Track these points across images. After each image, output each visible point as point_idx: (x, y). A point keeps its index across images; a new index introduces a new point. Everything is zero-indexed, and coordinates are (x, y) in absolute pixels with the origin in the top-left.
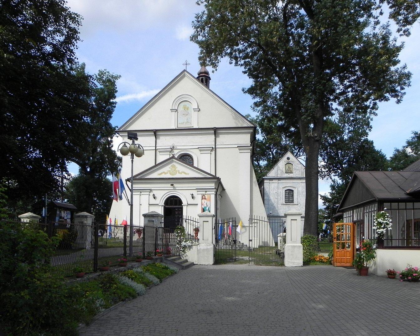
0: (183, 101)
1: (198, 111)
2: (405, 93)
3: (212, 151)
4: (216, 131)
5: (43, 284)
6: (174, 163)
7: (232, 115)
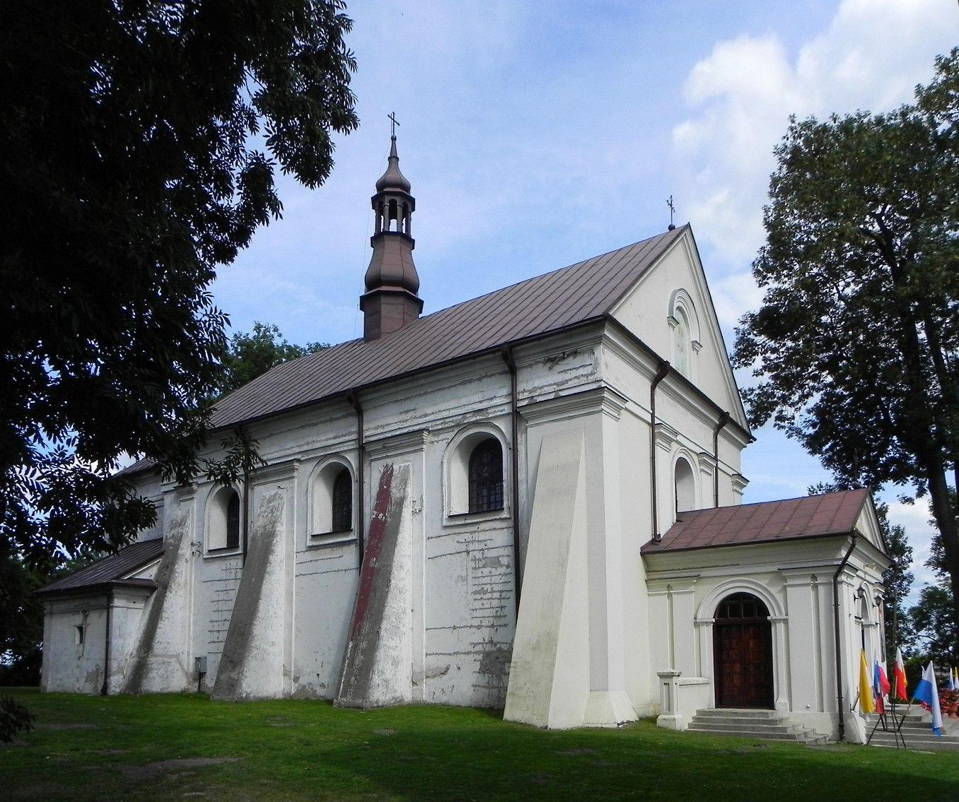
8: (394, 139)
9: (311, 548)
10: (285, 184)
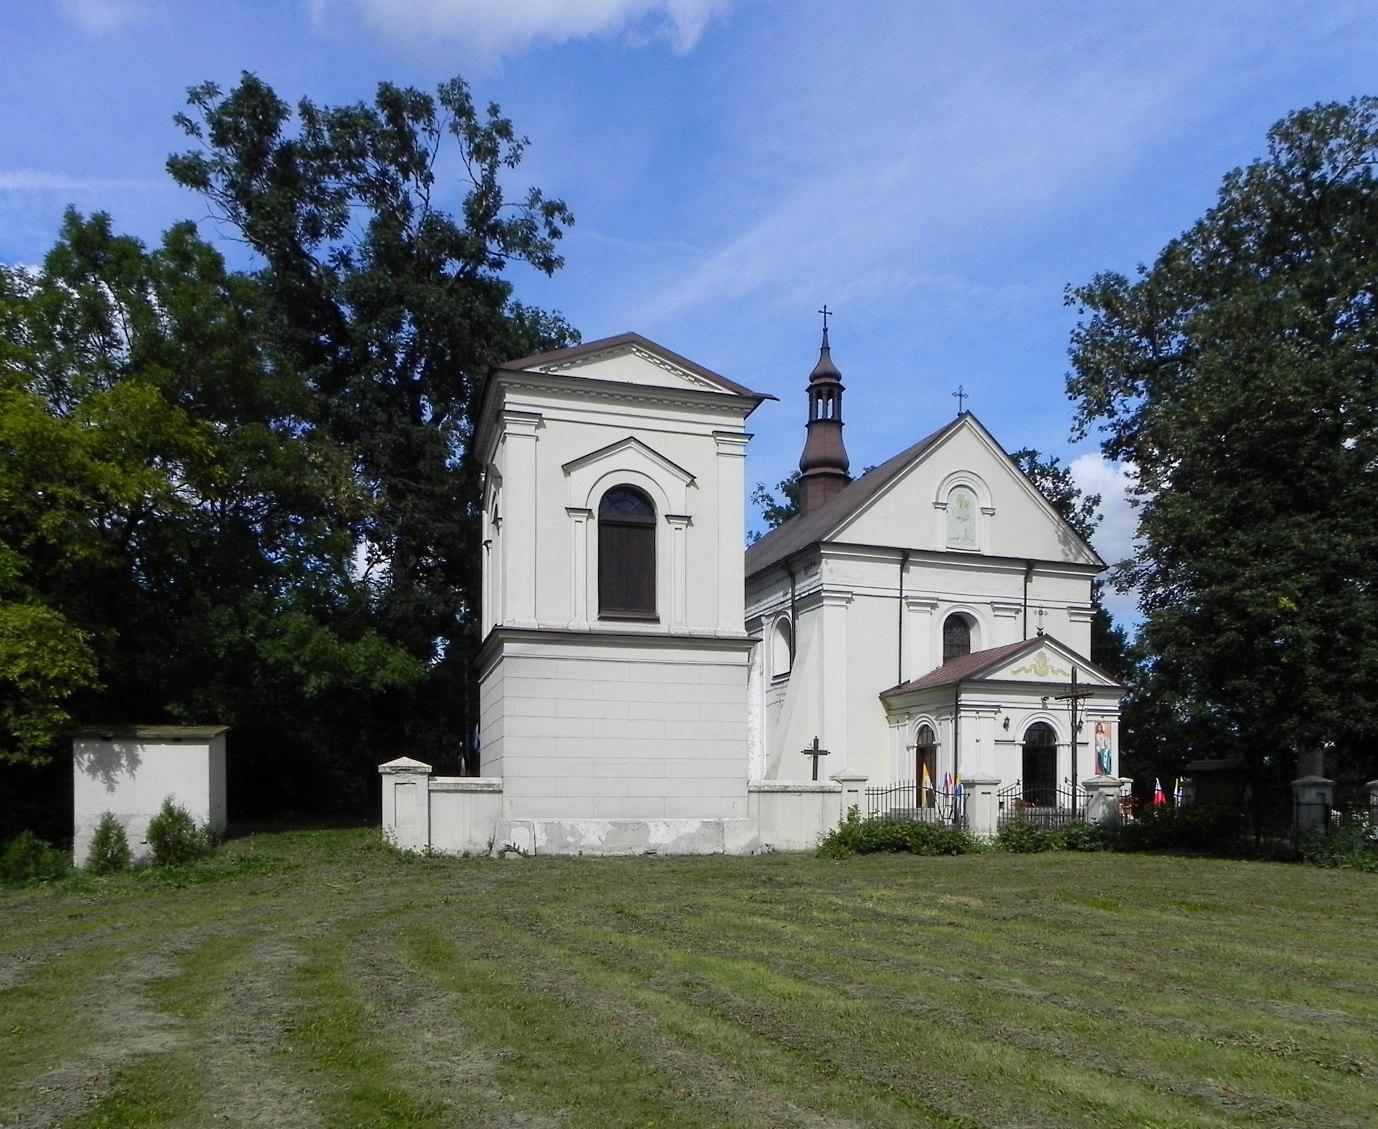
0: (961, 484)
1: (992, 515)
2: (1066, 393)
3: (1017, 612)
4: (1030, 567)
5: (1348, 778)
6: (1043, 650)
7: (1056, 532)
8: (825, 330)
9: (772, 684)
10: (1359, 98)
